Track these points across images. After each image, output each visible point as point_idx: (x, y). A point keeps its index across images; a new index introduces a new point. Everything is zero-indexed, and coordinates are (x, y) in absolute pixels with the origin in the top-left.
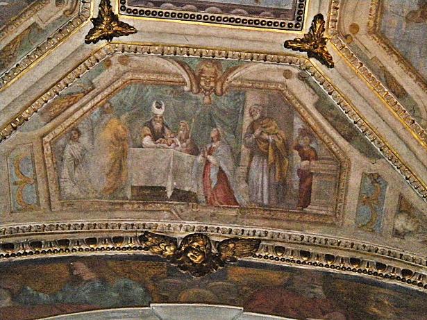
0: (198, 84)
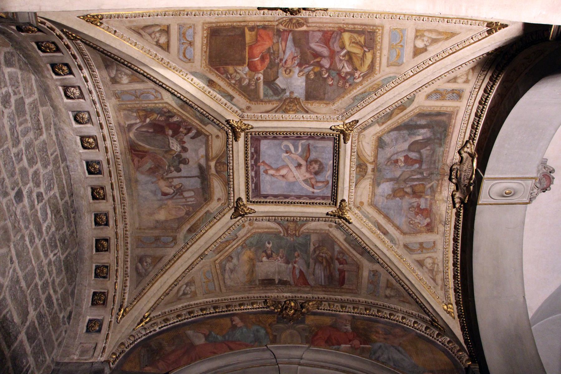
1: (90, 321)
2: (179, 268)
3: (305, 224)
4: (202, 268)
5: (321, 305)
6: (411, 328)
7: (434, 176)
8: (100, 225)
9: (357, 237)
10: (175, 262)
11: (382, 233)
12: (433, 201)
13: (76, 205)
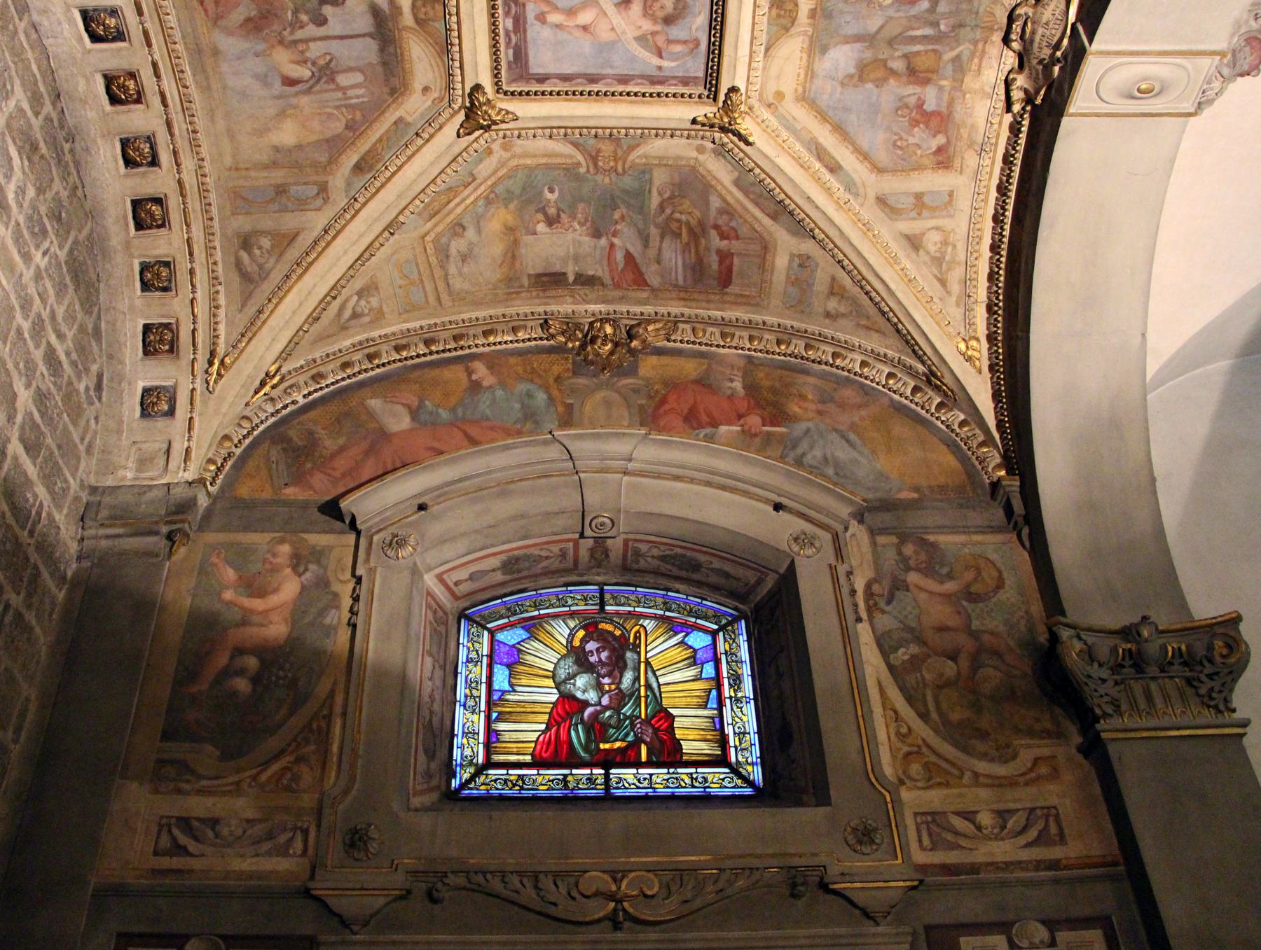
0: (596, 165)
1: (147, 391)
2: (339, 259)
3: (638, 145)
4: (392, 255)
5: (675, 329)
6: (880, 388)
7: (965, 33)
8: (137, 165)
9: (764, 176)
10: (328, 244)
11: (826, 167)
12: (958, 94)
13: (70, 121)
